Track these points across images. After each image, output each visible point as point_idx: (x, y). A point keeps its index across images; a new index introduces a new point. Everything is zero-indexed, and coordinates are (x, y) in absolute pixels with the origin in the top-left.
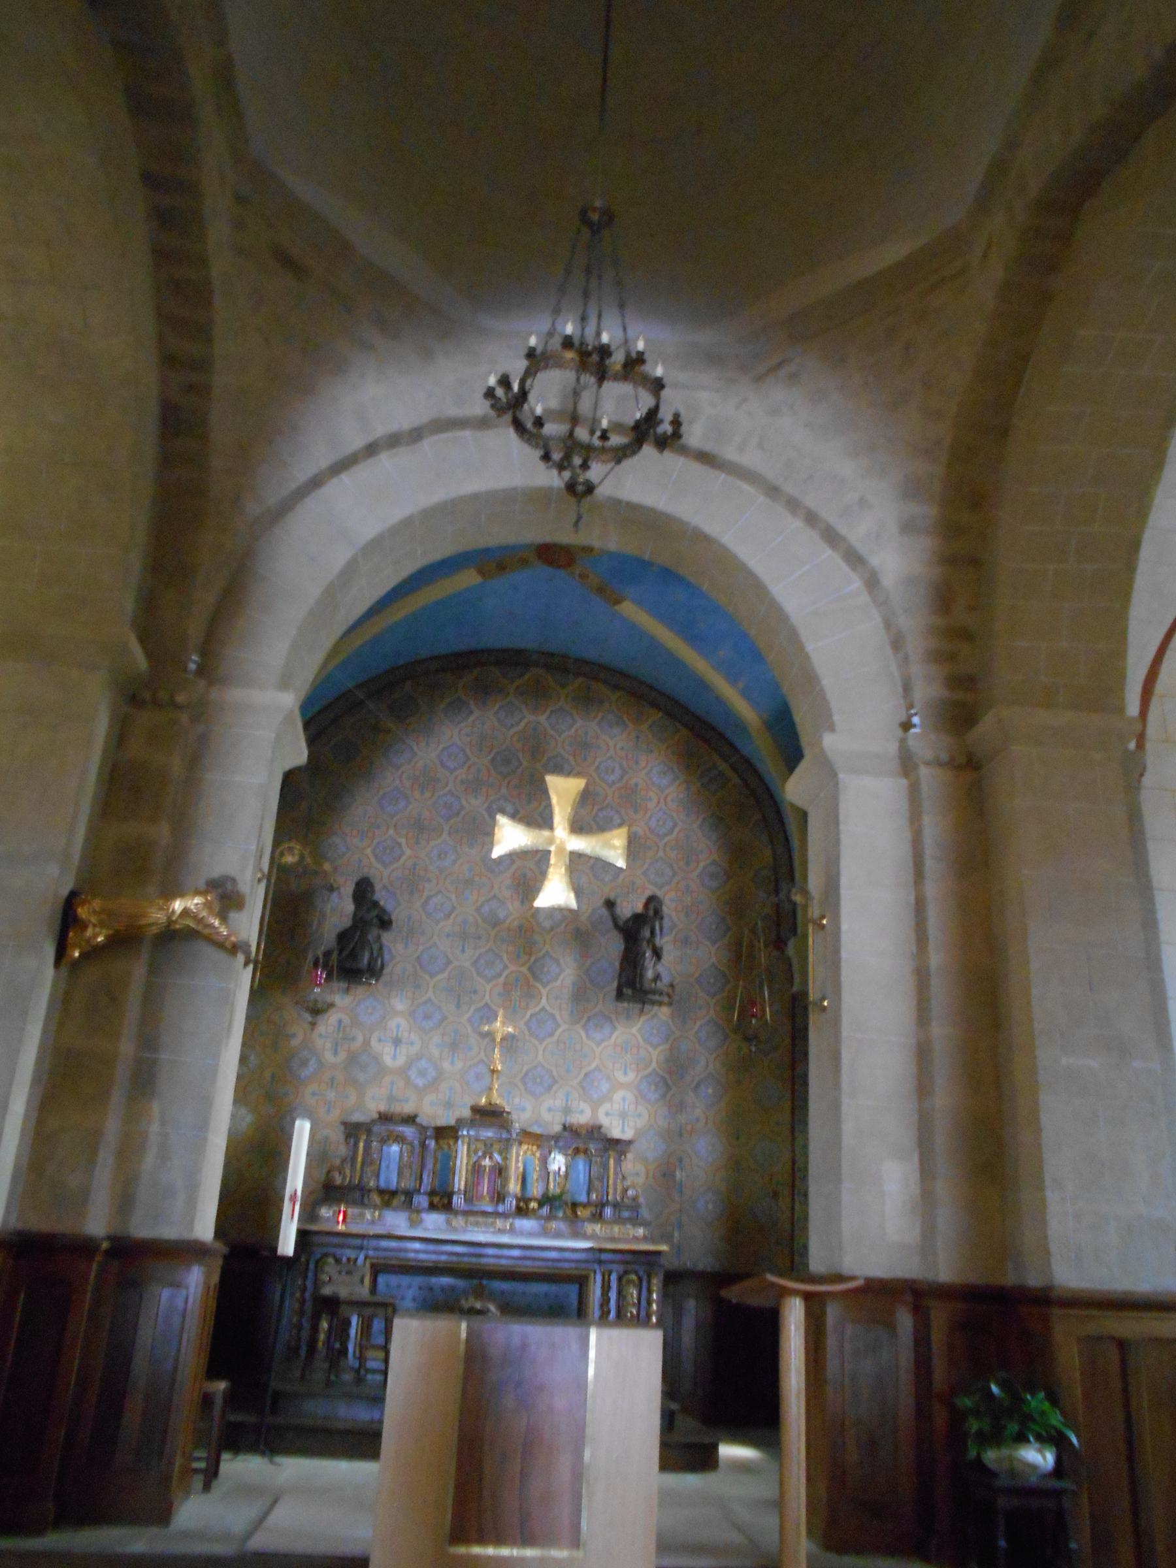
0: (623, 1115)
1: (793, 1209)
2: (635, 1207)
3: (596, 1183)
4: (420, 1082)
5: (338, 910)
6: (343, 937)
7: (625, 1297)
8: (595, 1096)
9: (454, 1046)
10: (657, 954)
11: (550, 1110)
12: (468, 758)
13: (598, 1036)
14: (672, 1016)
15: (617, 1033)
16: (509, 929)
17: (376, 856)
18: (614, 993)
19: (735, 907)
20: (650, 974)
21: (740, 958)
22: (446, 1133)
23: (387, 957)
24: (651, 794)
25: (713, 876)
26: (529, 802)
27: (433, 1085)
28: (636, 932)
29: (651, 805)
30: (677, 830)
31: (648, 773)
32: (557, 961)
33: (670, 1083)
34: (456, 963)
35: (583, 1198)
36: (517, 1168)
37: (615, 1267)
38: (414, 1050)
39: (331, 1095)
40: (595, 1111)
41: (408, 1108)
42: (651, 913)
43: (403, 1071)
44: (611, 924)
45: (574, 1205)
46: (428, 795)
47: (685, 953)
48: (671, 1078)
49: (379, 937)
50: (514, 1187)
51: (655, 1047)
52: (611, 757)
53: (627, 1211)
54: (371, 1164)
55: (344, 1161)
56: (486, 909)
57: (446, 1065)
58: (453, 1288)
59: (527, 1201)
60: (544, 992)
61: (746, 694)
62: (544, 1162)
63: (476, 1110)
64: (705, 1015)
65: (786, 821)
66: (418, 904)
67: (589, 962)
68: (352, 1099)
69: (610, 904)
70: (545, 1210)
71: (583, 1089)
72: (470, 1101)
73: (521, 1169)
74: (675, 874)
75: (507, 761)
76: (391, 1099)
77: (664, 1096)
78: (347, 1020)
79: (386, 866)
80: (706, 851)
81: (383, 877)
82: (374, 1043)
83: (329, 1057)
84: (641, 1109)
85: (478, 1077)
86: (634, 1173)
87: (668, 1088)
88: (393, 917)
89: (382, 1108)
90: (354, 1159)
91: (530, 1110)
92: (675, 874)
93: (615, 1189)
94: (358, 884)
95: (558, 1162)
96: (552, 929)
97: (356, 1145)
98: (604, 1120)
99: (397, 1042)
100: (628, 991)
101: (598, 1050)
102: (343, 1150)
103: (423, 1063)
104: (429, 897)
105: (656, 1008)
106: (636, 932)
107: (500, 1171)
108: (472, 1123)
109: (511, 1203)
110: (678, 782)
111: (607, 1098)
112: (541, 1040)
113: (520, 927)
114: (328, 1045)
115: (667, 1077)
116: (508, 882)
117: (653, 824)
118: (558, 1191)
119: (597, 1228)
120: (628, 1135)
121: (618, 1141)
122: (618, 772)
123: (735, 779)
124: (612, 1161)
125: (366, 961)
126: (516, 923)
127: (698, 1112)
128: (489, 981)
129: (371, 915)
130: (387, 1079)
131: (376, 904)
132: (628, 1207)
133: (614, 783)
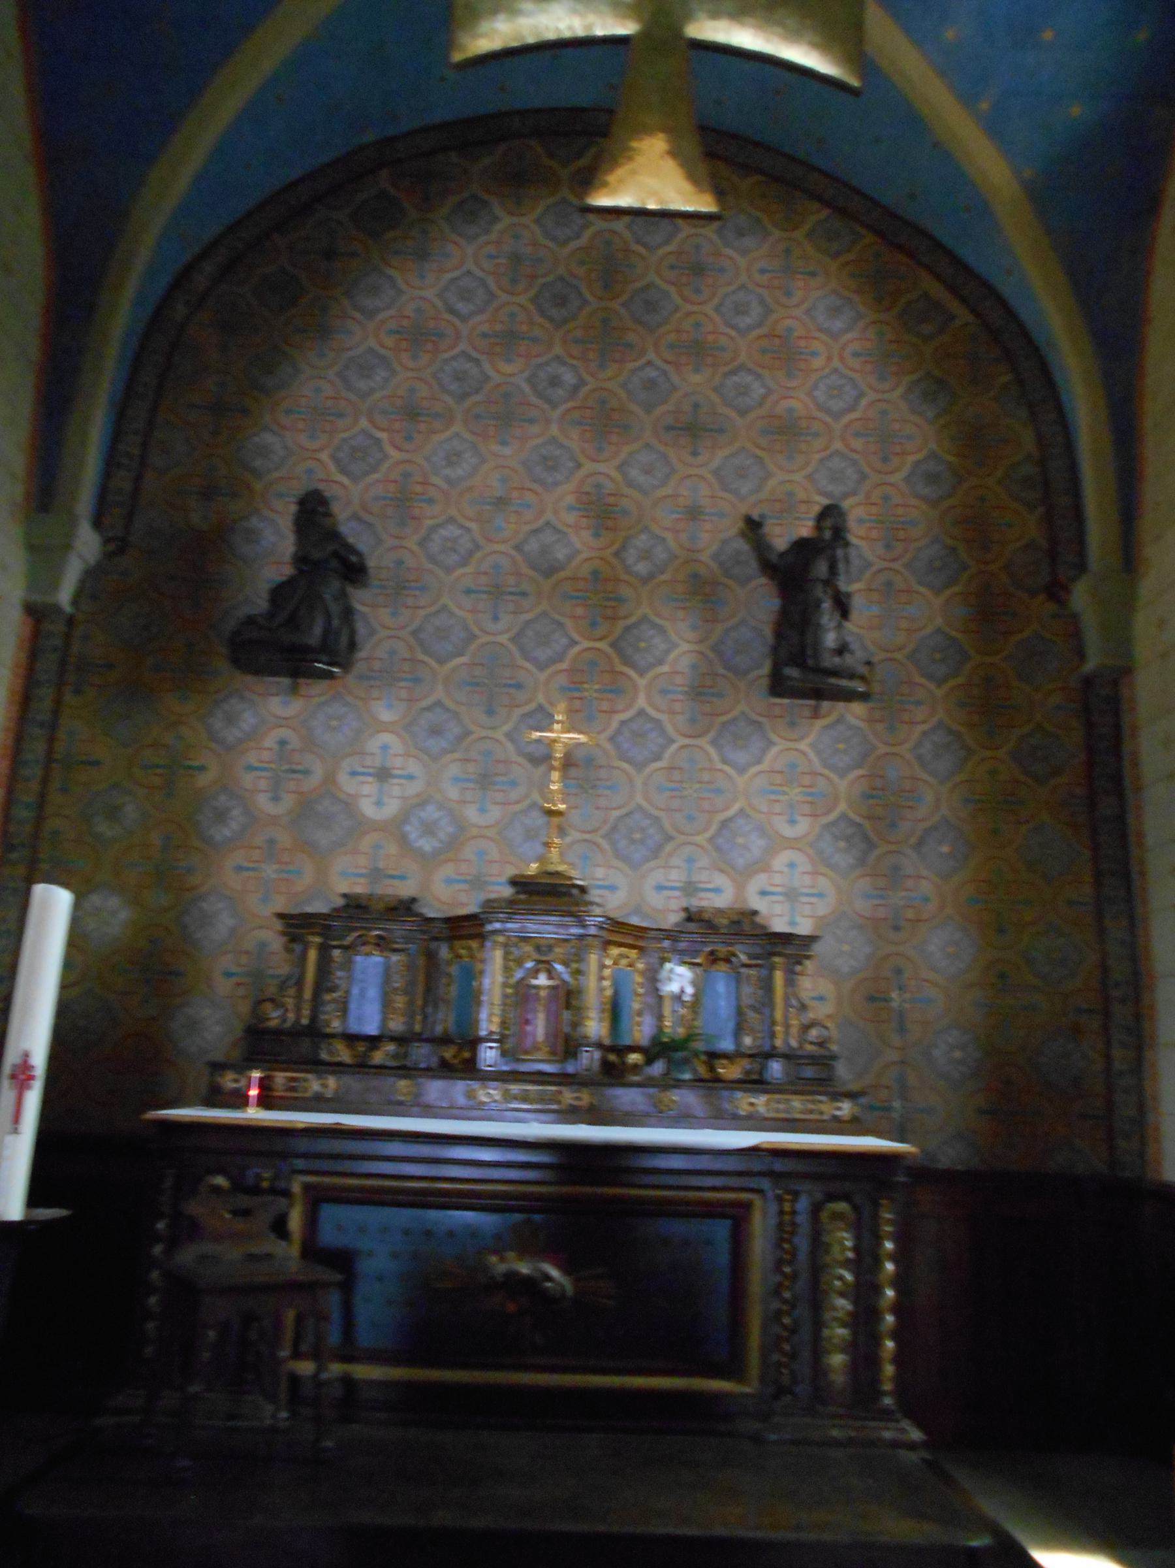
0: (791, 895)
1: (1108, 1057)
2: (824, 1061)
3: (751, 1015)
4: (426, 844)
5: (272, 548)
6: (278, 593)
7: (827, 1248)
8: (740, 862)
9: (485, 781)
10: (843, 607)
11: (660, 888)
12: (492, 296)
13: (741, 757)
14: (871, 721)
15: (774, 750)
16: (574, 579)
17: (337, 461)
18: (765, 682)
19: (973, 529)
20: (830, 639)
21: (988, 612)
22: (465, 928)
23: (361, 629)
24: (816, 346)
25: (932, 479)
26: (602, 366)
27: (452, 847)
28: (802, 575)
29: (817, 363)
30: (864, 402)
31: (808, 312)
32: (662, 631)
33: (872, 835)
34: (484, 639)
35: (727, 1045)
36: (601, 990)
37: (804, 1186)
38: (413, 788)
39: (270, 871)
40: (740, 887)
41: (405, 890)
42: (828, 534)
43: (395, 828)
44: (754, 565)
45: (713, 1056)
46: (425, 358)
47: (886, 613)
48: (872, 829)
49: (343, 595)
50: (595, 1027)
51: (842, 773)
52: (743, 287)
53: (814, 1073)
54: (333, 989)
55: (282, 986)
56: (533, 546)
57: (471, 813)
58: (473, 1232)
59: (622, 1051)
60: (642, 682)
61: (995, 128)
62: (653, 979)
63: (520, 884)
64: (930, 713)
65: (1059, 379)
66: (412, 543)
67: (719, 629)
68: (307, 877)
69: (753, 526)
70: (658, 1068)
71: (718, 849)
72: (511, 871)
73: (609, 993)
74: (863, 477)
75: (561, 301)
76: (376, 874)
77: (862, 861)
78: (295, 742)
79: (355, 479)
80: (919, 437)
81: (353, 502)
82: (343, 778)
83: (263, 802)
84: (823, 883)
85: (530, 834)
86: (818, 996)
87: (871, 845)
88: (371, 563)
89: (359, 889)
90: (300, 983)
91: (619, 888)
92: (863, 477)
93: (787, 1026)
94: (302, 502)
95: (679, 979)
96: (651, 577)
97: (304, 957)
98: (756, 903)
99: (383, 775)
100: (792, 672)
101: (741, 781)
102: (281, 966)
103: (431, 812)
104: (434, 528)
105: (841, 706)
106: (802, 575)
107: (568, 998)
108: (512, 908)
109: (589, 1059)
110: (861, 324)
111: (761, 866)
112: (640, 766)
113: (595, 573)
114: (263, 784)
115: (867, 825)
116: (570, 499)
117: (820, 394)
118: (681, 1031)
119: (761, 1103)
120: (804, 928)
121: (786, 938)
122: (756, 310)
123: (963, 315)
124: (779, 976)
125: (318, 630)
126: (585, 570)
127: (926, 887)
128: (542, 668)
129: (329, 560)
130: (366, 843)
131: (334, 535)
132: (814, 1060)
133: (750, 328)
